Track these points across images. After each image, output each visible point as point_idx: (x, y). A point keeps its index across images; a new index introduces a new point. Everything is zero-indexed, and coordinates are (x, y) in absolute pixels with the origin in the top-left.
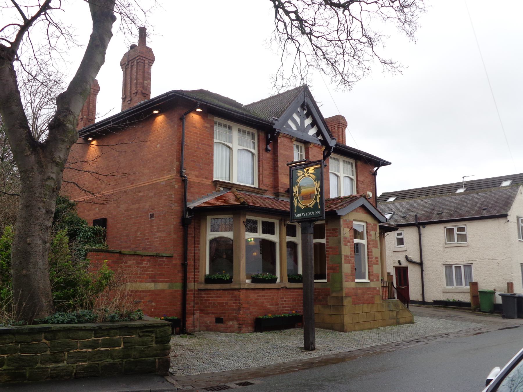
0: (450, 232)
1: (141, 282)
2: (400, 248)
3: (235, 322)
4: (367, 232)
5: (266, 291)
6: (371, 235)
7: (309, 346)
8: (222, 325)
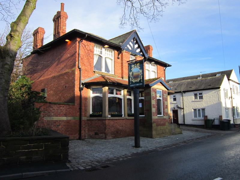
0: (196, 95)
1: (59, 116)
2: (175, 102)
3: (104, 134)
4: (163, 94)
5: (118, 121)
6: (164, 96)
7: (137, 145)
8: (97, 136)
